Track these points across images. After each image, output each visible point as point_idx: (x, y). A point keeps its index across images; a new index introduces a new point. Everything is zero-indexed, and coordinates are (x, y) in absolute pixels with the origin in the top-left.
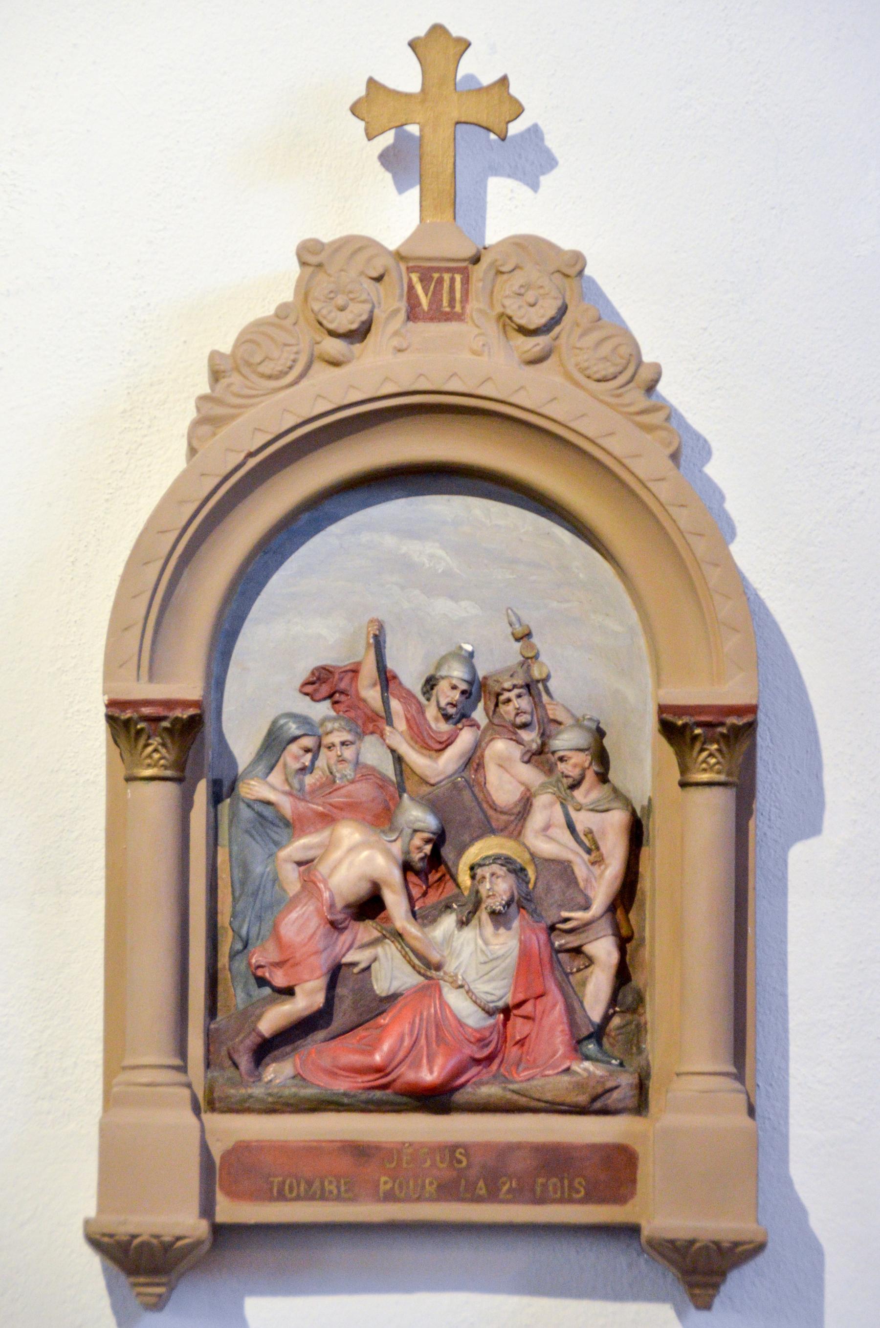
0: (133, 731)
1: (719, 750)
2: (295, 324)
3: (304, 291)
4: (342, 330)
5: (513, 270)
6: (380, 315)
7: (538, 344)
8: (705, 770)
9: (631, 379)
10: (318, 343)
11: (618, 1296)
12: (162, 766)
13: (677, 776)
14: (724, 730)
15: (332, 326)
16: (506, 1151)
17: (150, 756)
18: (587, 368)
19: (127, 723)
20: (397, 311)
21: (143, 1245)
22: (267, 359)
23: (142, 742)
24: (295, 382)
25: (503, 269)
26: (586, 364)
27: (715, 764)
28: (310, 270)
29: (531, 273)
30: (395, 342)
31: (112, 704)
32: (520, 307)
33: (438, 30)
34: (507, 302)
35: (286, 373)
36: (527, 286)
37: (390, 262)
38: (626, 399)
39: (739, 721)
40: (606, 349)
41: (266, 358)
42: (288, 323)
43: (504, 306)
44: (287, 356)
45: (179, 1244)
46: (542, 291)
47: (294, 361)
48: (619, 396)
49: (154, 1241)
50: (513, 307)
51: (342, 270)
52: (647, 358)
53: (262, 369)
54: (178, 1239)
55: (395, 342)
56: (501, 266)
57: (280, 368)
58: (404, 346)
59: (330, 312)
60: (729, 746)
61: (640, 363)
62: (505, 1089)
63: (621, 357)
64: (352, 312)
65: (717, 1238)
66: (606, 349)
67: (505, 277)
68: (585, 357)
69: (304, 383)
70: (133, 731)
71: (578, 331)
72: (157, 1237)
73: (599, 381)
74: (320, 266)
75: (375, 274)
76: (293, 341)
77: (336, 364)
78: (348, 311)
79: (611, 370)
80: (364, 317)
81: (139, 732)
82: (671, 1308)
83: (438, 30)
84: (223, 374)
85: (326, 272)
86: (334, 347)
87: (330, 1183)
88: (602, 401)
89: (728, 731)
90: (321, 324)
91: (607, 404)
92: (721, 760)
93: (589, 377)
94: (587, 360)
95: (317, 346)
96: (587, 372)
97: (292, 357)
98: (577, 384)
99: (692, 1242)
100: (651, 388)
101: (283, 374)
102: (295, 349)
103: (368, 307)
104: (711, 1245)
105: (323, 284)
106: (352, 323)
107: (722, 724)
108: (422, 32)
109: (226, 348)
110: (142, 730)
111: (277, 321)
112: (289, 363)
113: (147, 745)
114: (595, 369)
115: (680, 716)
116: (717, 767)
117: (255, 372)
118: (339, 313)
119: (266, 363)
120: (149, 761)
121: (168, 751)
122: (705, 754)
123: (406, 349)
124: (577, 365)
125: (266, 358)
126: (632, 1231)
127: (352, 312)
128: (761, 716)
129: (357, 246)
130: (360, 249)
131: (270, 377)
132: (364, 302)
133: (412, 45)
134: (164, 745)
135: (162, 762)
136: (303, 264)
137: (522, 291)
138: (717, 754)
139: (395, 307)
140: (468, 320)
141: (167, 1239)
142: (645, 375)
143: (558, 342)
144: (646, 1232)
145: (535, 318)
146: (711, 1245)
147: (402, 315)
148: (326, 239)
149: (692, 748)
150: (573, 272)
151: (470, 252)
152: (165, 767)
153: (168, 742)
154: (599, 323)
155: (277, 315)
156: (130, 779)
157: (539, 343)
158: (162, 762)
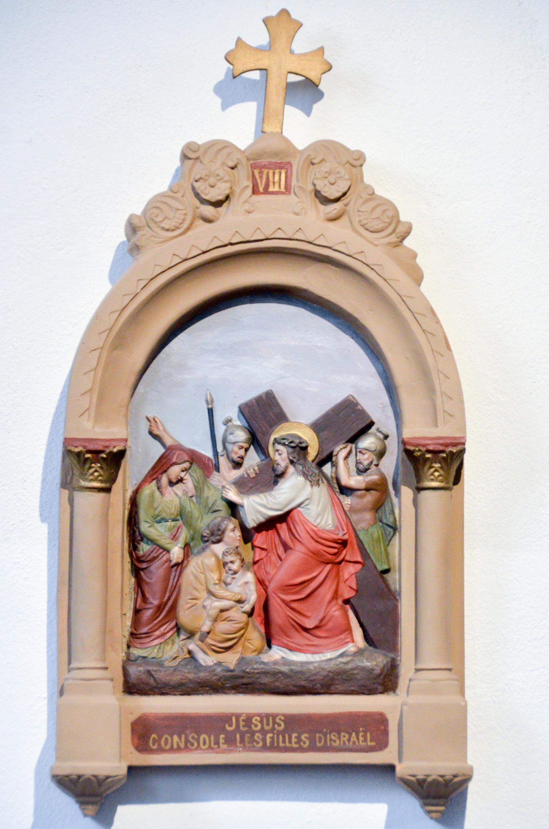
0: (82, 459)
2: (183, 196)
4: (213, 200)
5: (321, 162)
6: (237, 190)
7: (335, 209)
8: (432, 480)
9: (394, 231)
10: (198, 208)
11: (464, 807)
12: (100, 480)
14: (445, 455)
16: (266, 717)
17: (92, 474)
19: (79, 454)
20: (247, 187)
21: (434, 780)
22: (167, 219)
23: (87, 466)
24: (188, 229)
25: (314, 161)
26: (366, 222)
27: (439, 476)
30: (247, 207)
32: (325, 185)
33: (284, 13)
36: (329, 173)
39: (454, 450)
40: (377, 213)
41: (166, 218)
42: (178, 195)
44: (179, 216)
45: (456, 780)
46: (338, 175)
49: (440, 779)
51: (212, 161)
52: (403, 218)
53: (163, 225)
54: (455, 776)
56: (313, 159)
57: (174, 224)
58: (252, 209)
59: (205, 188)
60: (447, 464)
61: (399, 222)
64: (219, 188)
65: (95, 773)
66: (377, 213)
69: (190, 233)
70: (82, 459)
71: (360, 201)
72: (442, 776)
73: (371, 232)
74: (197, 158)
75: (232, 164)
76: (180, 207)
77: (208, 221)
78: (251, 215)
79: (381, 226)
83: (284, 13)
84: (139, 229)
85: (201, 162)
86: (208, 211)
87: (344, 736)
89: (447, 455)
93: (367, 229)
94: (366, 219)
95: (197, 210)
96: (366, 226)
97: (182, 217)
98: (361, 235)
99: (79, 777)
102: (184, 212)
103: (228, 185)
104: (93, 778)
105: (199, 171)
107: (443, 452)
109: (139, 211)
110: (88, 458)
111: (172, 194)
114: (371, 224)
116: (440, 478)
117: (159, 227)
118: (211, 189)
119: (166, 221)
121: (104, 471)
122: (432, 470)
123: (252, 212)
124: (360, 221)
125: (166, 218)
126: (390, 769)
128: (467, 446)
129: (223, 145)
130: (225, 147)
131: (168, 230)
132: (226, 181)
133: (266, 21)
134: (101, 468)
135: (100, 478)
137: (327, 175)
138: (439, 469)
139: (244, 185)
140: (292, 191)
141: (421, 777)
142: (401, 229)
143: (348, 208)
144: (401, 770)
145: (332, 193)
146: (93, 778)
147: (250, 191)
148: (200, 142)
149: (424, 465)
152: (101, 481)
153: (105, 466)
154: (373, 196)
155: (171, 189)
157: (337, 206)
158: (100, 478)
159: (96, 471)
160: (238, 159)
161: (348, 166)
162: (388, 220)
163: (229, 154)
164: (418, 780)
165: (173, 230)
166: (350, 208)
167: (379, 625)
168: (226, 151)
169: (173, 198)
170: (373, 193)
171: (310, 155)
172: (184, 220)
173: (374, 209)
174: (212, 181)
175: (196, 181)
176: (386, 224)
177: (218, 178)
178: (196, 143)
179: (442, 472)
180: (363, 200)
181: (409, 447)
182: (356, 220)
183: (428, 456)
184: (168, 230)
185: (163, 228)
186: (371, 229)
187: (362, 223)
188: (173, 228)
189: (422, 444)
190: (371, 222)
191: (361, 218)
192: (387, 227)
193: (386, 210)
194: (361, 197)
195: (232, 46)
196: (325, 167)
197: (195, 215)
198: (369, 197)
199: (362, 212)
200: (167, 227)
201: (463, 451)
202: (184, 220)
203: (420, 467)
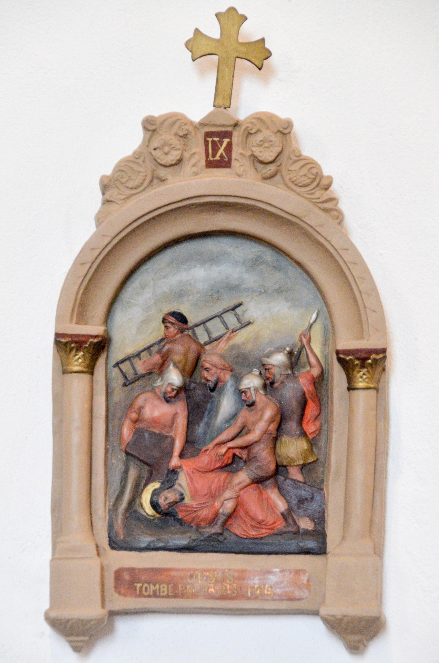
1: (368, 371)
3: (147, 142)
7: (270, 170)
9: (318, 185)
13: (346, 385)
15: (163, 162)
18: (295, 181)
19: (66, 344)
25: (252, 132)
26: (295, 178)
27: (366, 378)
28: (150, 133)
29: (266, 134)
31: (58, 335)
33: (232, 10)
34: (254, 149)
35: (142, 183)
37: (191, 129)
38: (317, 195)
40: (304, 171)
42: (140, 161)
43: (252, 151)
46: (271, 143)
47: (146, 176)
48: (312, 194)
50: (257, 151)
55: (194, 169)
56: (251, 130)
61: (322, 177)
62: (281, 588)
63: (313, 174)
64: (172, 155)
66: (304, 171)
67: (253, 136)
68: (295, 175)
70: (68, 349)
74: (154, 131)
75: (181, 134)
76: (143, 170)
78: (169, 155)
79: (308, 181)
80: (178, 158)
81: (72, 349)
82: (241, 445)
83: (232, 10)
88: (303, 197)
90: (155, 160)
91: (306, 198)
92: (369, 376)
93: (296, 185)
96: (296, 182)
98: (292, 190)
100: (327, 188)
101: (138, 187)
103: (179, 152)
106: (173, 161)
108: (223, 10)
109: (108, 172)
112: (141, 182)
113: (76, 355)
114: (299, 181)
115: (349, 355)
120: (76, 363)
124: (290, 179)
127: (172, 155)
131: (132, 188)
132: (179, 149)
134: (368, 371)
136: (145, 128)
137: (262, 143)
138: (367, 373)
141: (339, 617)
143: (280, 167)
144: (323, 611)
145: (268, 156)
150: (286, 131)
151: (233, 123)
156: (65, 372)
157: (272, 168)
159: (364, 374)
160: (187, 130)
161: (279, 134)
162: (314, 177)
163: (180, 127)
164: (337, 619)
165: (135, 189)
166: (283, 168)
167: (289, 498)
168: (178, 124)
169: (136, 163)
170: (300, 156)
171: (248, 127)
172: (144, 180)
173: (301, 168)
174: (166, 149)
175: (155, 149)
176: (312, 180)
177: (171, 147)
178: (153, 117)
179: (368, 375)
180: (292, 161)
181: (342, 356)
182: (287, 178)
183: (357, 362)
184: (132, 188)
185: (127, 187)
186: (300, 184)
187: (292, 180)
188: (134, 187)
189: (147, 347)
190: (299, 179)
191: (291, 176)
192: (312, 182)
193: (311, 168)
194: (291, 159)
195: (191, 35)
196: (260, 137)
197: (153, 176)
198: (297, 158)
199: (291, 171)
200: (131, 186)
201: (385, 358)
202: (144, 180)
203: (350, 371)
